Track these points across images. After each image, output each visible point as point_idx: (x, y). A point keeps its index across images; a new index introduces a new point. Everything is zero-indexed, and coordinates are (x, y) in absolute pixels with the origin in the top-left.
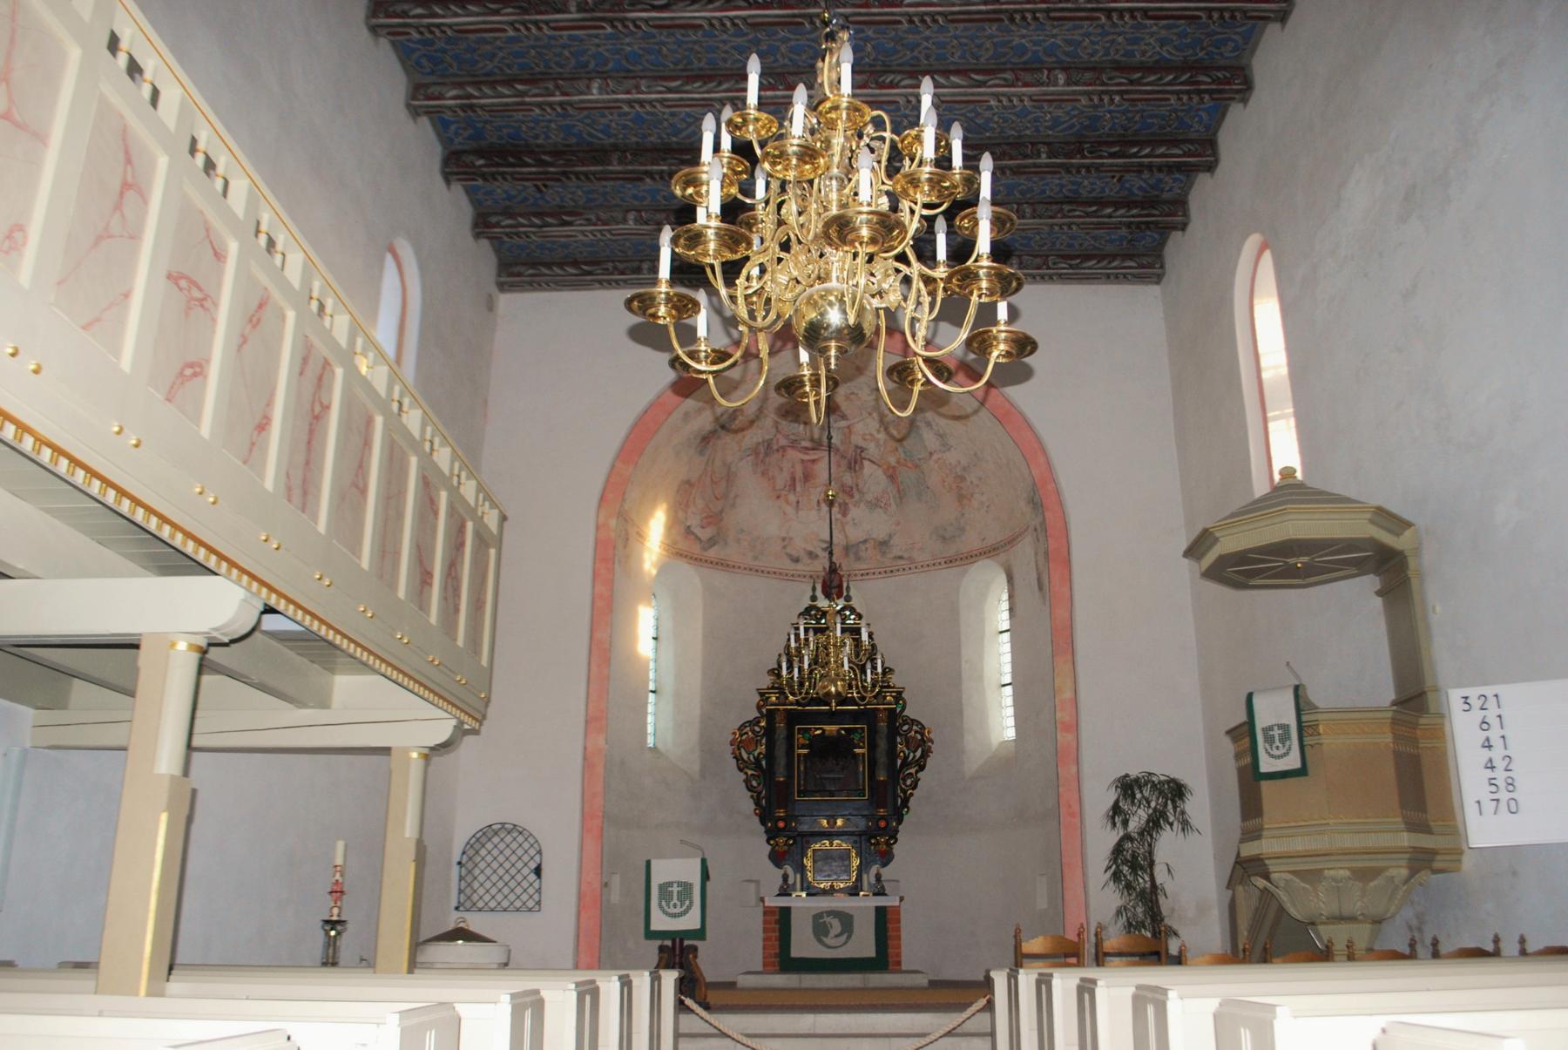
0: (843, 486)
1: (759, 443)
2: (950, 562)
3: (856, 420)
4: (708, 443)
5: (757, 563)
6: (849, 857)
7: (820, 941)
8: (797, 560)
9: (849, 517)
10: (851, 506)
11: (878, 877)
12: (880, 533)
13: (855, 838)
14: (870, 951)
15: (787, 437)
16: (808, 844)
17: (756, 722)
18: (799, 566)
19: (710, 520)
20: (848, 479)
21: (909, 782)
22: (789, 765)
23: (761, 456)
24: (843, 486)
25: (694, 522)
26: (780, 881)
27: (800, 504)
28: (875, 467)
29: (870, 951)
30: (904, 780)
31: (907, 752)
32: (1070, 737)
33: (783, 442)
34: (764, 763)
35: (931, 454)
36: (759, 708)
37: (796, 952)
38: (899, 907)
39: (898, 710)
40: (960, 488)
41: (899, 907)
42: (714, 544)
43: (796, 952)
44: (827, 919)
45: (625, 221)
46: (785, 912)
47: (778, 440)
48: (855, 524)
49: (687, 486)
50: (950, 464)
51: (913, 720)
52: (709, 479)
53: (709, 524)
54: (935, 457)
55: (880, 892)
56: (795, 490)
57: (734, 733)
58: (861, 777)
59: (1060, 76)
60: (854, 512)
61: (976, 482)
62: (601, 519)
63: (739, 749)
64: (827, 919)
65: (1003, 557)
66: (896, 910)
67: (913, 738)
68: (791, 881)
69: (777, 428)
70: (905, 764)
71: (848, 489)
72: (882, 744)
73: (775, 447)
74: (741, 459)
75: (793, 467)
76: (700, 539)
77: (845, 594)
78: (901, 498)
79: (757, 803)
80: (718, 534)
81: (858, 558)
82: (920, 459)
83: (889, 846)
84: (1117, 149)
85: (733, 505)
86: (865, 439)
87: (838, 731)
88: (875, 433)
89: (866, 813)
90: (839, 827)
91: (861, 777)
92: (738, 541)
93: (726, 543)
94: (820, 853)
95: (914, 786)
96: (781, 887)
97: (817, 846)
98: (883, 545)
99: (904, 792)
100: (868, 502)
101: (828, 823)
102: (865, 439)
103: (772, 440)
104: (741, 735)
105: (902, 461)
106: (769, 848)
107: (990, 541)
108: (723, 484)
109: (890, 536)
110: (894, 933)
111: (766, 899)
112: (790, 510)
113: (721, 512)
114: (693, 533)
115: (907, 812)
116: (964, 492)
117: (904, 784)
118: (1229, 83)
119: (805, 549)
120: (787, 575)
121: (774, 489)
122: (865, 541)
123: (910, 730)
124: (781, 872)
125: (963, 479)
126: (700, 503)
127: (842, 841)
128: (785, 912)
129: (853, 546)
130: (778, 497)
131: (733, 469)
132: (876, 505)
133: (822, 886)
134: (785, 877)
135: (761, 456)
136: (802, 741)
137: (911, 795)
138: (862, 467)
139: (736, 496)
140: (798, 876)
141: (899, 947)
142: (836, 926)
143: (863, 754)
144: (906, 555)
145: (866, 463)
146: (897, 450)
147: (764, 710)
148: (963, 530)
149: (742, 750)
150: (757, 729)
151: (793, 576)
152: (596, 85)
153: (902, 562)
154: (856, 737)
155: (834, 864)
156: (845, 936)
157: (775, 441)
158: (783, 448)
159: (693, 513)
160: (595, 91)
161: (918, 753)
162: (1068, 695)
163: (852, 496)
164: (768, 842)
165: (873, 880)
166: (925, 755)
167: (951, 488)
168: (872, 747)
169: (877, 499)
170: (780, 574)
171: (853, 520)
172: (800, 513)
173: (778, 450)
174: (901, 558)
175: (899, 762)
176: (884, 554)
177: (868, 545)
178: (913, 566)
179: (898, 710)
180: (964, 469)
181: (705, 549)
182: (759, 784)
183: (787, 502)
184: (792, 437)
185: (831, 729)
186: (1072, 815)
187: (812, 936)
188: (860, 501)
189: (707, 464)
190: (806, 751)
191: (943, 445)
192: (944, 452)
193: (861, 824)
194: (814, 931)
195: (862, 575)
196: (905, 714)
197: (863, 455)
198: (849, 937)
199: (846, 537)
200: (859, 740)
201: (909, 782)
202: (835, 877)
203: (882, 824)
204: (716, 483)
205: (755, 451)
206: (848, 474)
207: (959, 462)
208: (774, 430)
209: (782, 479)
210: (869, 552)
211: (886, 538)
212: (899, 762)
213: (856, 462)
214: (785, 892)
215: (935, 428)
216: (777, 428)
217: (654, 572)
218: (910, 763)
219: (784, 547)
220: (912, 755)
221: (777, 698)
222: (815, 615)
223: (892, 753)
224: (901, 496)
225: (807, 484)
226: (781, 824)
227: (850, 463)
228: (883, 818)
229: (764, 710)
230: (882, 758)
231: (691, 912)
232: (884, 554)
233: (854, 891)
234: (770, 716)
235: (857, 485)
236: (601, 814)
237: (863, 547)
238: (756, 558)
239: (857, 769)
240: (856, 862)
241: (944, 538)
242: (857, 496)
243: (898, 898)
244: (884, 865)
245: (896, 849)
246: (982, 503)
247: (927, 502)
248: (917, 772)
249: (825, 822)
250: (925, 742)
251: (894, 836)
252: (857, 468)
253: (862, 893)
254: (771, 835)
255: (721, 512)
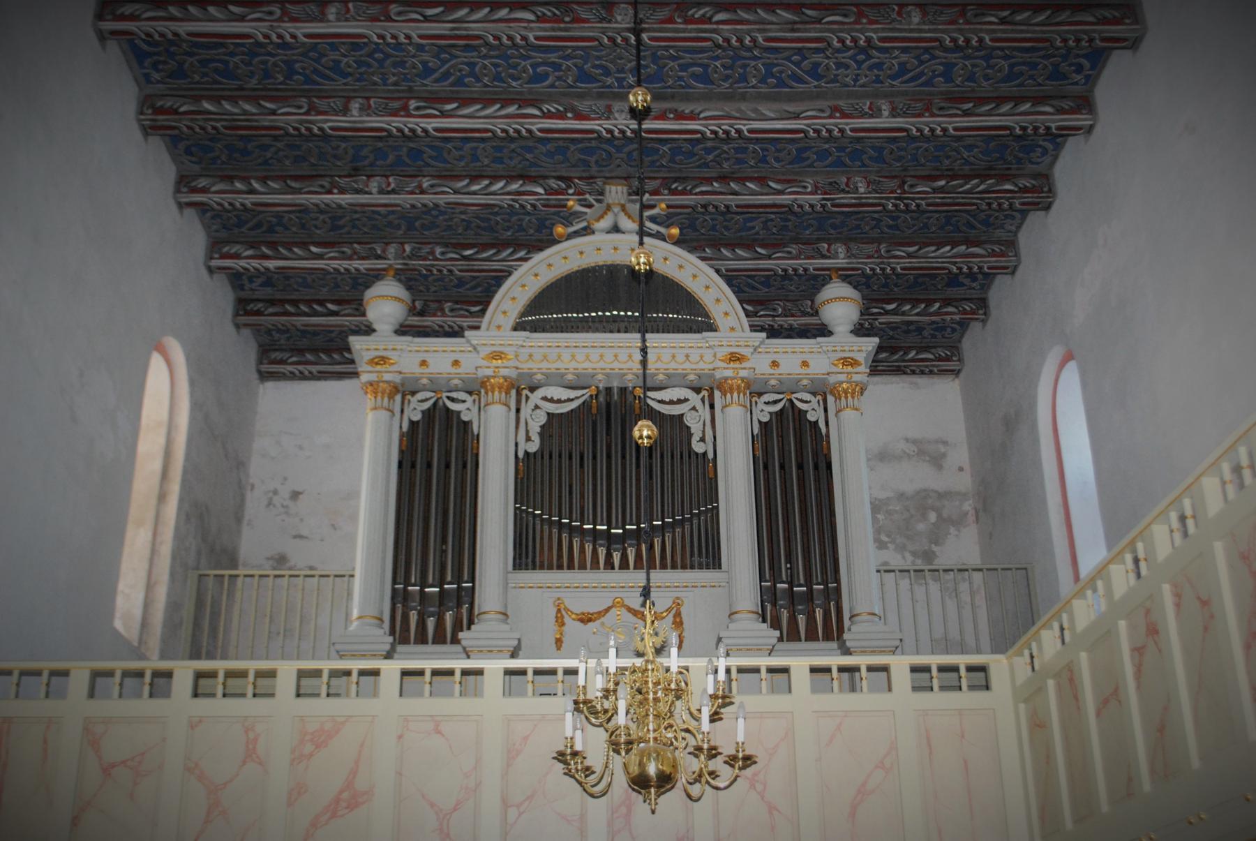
45: (345, 111)
59: (840, 250)
84: (942, 183)
118: (974, 313)
152: (392, 250)
160: (355, 112)
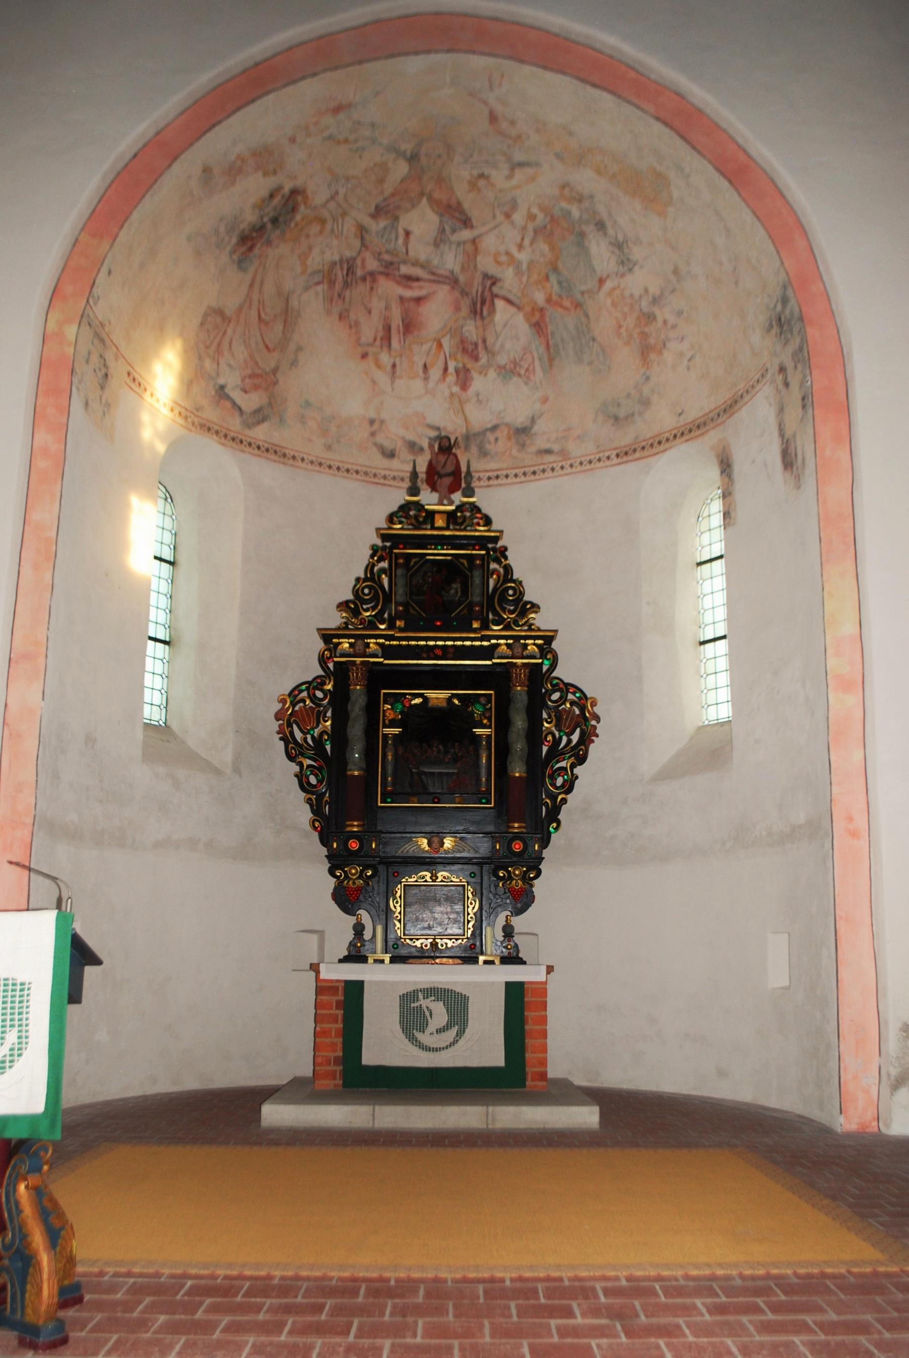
0: (463, 341)
1: (334, 264)
2: (625, 454)
3: (487, 228)
4: (251, 249)
5: (329, 455)
6: (463, 899)
7: (413, 1039)
8: (391, 455)
9: (471, 391)
10: (474, 374)
11: (508, 932)
12: (519, 417)
13: (475, 869)
14: (495, 1057)
15: (378, 256)
16: (397, 877)
17: (315, 684)
18: (395, 464)
19: (257, 381)
20: (471, 330)
21: (559, 781)
22: (370, 754)
23: (338, 286)
24: (463, 341)
25: (231, 379)
26: (350, 935)
27: (398, 368)
28: (513, 310)
29: (495, 1057)
30: (553, 778)
31: (557, 734)
32: (852, 700)
33: (372, 264)
34: (328, 747)
35: (601, 281)
36: (322, 661)
37: (370, 1057)
38: (546, 983)
39: (545, 668)
40: (644, 335)
41: (546, 983)
42: (263, 420)
43: (370, 1057)
44: (424, 1003)
46: (355, 989)
47: (363, 261)
48: (479, 402)
49: (219, 319)
50: (632, 296)
51: (568, 685)
52: (254, 313)
53: (256, 387)
54: (608, 285)
55: (512, 959)
56: (390, 345)
57: (283, 701)
58: (483, 771)
60: (478, 383)
61: (671, 319)
62: (51, 325)
63: (290, 725)
64: (424, 1003)
65: (713, 437)
66: (541, 989)
67: (570, 711)
68: (367, 935)
69: (362, 239)
70: (555, 753)
71: (470, 348)
72: (519, 722)
73: (359, 273)
74: (307, 288)
75: (386, 308)
76: (240, 409)
77: (463, 485)
78: (551, 360)
79: (316, 810)
80: (270, 405)
81: (484, 453)
82: (583, 293)
83: (528, 881)
85: (294, 363)
86: (498, 263)
87: (449, 700)
88: (514, 251)
89: (491, 828)
90: (446, 852)
91: (483, 771)
92: (302, 419)
93: (282, 420)
94: (415, 891)
95: (569, 787)
96: (352, 944)
97: (412, 880)
98: (522, 433)
99: (554, 797)
100: (501, 368)
101: (429, 844)
102: (498, 263)
103: (355, 259)
104: (293, 704)
105: (554, 298)
106: (332, 882)
107: (694, 413)
108: (279, 327)
109: (533, 420)
110: (538, 1027)
111: (322, 967)
112: (382, 378)
113: (275, 371)
114: (228, 398)
115: (556, 829)
116: (652, 341)
117: (554, 785)
119: (403, 438)
120: (375, 475)
121: (358, 342)
122: (495, 428)
123: (563, 700)
124: (352, 920)
125: (650, 318)
126: (241, 352)
127: (449, 871)
128: (355, 989)
129: (474, 435)
130: (364, 356)
131: (294, 303)
132: (512, 372)
133: (418, 944)
134: (359, 929)
135: (338, 286)
136: (390, 715)
137: (564, 801)
138: (493, 310)
139: (299, 349)
140: (379, 929)
141: (544, 1049)
142: (439, 1014)
143: (489, 737)
144: (556, 447)
145: (500, 304)
146: (547, 278)
147: (331, 665)
148: (646, 403)
149: (295, 726)
150: (319, 694)
151: (385, 477)
153: (549, 458)
154: (478, 710)
155: (438, 909)
156: (455, 1030)
157: (359, 262)
158: (372, 274)
159: (230, 366)
161: (575, 738)
162: (849, 628)
163: (476, 358)
164: (331, 872)
165: (500, 935)
166: (587, 739)
167: (631, 336)
168: (503, 725)
169: (515, 363)
170: (366, 474)
171: (478, 395)
172: (397, 381)
173: (364, 279)
174: (548, 452)
175: (545, 749)
176: (523, 446)
177: (498, 433)
178: (566, 464)
179: (545, 668)
180: (655, 301)
181: (249, 426)
182: (320, 782)
183: (378, 366)
184: (387, 257)
185: (438, 696)
186: (854, 834)
187: (397, 1028)
188: (489, 365)
189: (251, 285)
190: (396, 731)
191: (622, 263)
192: (623, 275)
193: (483, 847)
194: (402, 1023)
195: (489, 478)
196: (554, 674)
197: (495, 290)
198: (461, 1033)
199: (466, 420)
200: (483, 714)
201: (559, 781)
202: (440, 929)
203: (517, 847)
204: (267, 324)
205: (327, 276)
206: (473, 322)
207: (646, 291)
208: (357, 243)
209: (370, 329)
210: (500, 443)
211: (528, 423)
212: (545, 749)
213: (483, 303)
214: (355, 956)
215: (611, 232)
216: (362, 239)
217: (161, 448)
218: (562, 753)
219: (373, 434)
220: (565, 739)
221: (351, 645)
222: (416, 517)
223: (534, 735)
224: (551, 356)
225: (410, 338)
226: (354, 845)
227: (474, 304)
228: (517, 836)
229: (331, 665)
230: (519, 746)
231: (19, 1064)
232: (523, 446)
233: (469, 956)
234: (341, 674)
235: (484, 341)
236: (29, 821)
237: (491, 437)
238: (329, 448)
239: (478, 758)
240: (473, 908)
241: (616, 419)
242: (484, 359)
243: (544, 969)
244: (519, 912)
245: (539, 887)
246: (681, 354)
247: (590, 363)
248: (573, 766)
249: (424, 843)
250: (586, 720)
251: (534, 866)
252: (485, 312)
253: (482, 958)
254: (336, 862)
255: (275, 371)
